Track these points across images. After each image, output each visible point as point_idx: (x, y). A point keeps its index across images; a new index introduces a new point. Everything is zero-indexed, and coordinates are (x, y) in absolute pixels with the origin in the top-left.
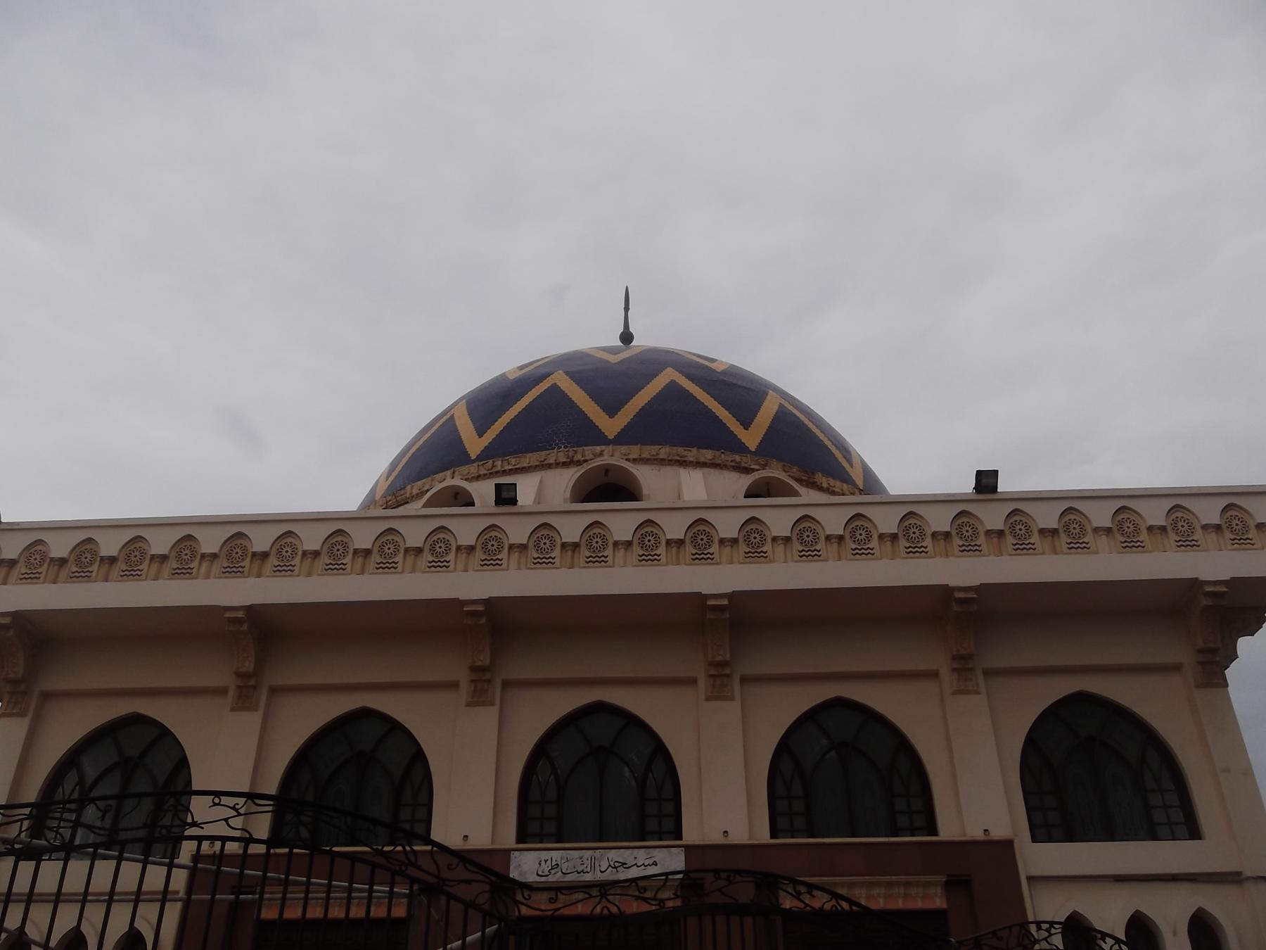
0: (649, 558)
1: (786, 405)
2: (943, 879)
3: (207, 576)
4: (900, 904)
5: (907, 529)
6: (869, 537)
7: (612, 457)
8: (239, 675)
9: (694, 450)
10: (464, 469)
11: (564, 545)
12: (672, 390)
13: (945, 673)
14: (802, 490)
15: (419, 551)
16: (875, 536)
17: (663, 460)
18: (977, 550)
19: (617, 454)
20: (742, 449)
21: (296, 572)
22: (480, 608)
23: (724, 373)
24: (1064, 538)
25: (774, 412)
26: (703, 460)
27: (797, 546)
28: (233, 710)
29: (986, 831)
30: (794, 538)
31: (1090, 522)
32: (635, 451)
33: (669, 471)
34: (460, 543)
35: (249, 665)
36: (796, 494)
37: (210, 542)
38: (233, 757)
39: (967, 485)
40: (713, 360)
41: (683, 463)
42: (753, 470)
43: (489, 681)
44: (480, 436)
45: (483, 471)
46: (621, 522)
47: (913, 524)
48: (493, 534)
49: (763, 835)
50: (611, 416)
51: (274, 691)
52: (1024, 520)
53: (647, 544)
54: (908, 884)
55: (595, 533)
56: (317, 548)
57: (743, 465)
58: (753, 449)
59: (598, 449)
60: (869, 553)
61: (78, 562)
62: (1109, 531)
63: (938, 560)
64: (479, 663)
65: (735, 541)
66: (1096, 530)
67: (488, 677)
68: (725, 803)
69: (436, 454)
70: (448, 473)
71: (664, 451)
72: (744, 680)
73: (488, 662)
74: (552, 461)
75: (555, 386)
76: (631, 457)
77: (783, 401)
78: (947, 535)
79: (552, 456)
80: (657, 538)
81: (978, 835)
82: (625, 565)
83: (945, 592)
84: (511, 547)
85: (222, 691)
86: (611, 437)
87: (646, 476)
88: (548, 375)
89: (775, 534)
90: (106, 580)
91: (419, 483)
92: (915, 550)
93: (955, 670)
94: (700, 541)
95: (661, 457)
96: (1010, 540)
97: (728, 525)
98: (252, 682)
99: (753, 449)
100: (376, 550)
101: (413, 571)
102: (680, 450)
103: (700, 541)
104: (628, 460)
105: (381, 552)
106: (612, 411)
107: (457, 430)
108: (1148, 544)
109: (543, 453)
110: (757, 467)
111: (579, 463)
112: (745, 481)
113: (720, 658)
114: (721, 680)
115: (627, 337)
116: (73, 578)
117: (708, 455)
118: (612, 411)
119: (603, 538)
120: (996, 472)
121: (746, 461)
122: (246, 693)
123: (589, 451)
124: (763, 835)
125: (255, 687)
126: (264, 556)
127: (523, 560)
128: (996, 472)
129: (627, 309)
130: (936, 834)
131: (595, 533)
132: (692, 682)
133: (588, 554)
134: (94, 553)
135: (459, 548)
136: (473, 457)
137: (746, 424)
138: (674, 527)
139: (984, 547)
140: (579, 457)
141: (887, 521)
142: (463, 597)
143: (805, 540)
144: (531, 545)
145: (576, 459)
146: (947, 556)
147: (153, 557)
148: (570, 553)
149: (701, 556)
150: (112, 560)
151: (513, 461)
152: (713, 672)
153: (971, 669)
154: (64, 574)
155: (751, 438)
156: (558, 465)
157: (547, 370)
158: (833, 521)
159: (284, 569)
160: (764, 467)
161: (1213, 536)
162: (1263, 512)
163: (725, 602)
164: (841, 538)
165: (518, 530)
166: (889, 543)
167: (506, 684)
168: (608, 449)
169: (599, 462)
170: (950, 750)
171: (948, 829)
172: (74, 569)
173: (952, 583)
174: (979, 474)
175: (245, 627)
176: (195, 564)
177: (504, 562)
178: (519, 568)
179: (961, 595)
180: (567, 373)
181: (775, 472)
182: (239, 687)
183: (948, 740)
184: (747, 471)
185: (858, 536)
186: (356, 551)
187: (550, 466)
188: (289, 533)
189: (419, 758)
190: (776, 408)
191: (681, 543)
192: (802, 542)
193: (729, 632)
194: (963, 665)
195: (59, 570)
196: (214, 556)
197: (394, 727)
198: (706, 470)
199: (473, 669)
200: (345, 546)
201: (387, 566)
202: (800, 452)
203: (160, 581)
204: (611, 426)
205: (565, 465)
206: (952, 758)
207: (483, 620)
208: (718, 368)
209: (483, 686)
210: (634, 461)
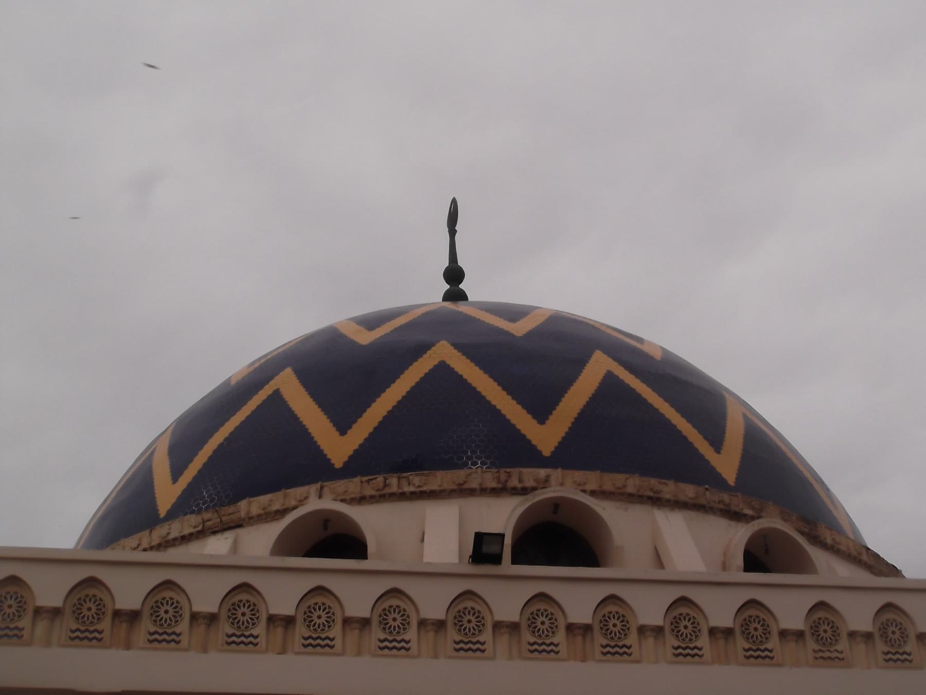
3: (48, 644)
7: (564, 486)
9: (671, 483)
14: (816, 554)
16: (775, 633)
17: (631, 495)
21: (182, 645)
25: (742, 431)
26: (682, 498)
27: (452, 634)
30: (596, 628)
31: (913, 623)
32: (593, 479)
41: (656, 501)
45: (369, 491)
52: (831, 618)
55: (753, 615)
56: (214, 609)
57: (733, 508)
60: (403, 648)
62: (868, 636)
66: (852, 635)
70: (313, 489)
71: (633, 483)
74: (474, 484)
75: (442, 370)
76: (590, 487)
78: (587, 628)
80: (177, 608)
86: (338, 463)
87: (371, 520)
88: (420, 350)
95: (630, 489)
97: (720, 609)
100: (146, 612)
102: (653, 482)
104: (584, 491)
106: (542, 412)
107: (295, 418)
108: (707, 652)
110: (749, 512)
111: (524, 491)
118: (541, 413)
126: (133, 616)
129: (452, 232)
131: (753, 615)
133: (605, 642)
139: (563, 648)
140: (514, 482)
146: (584, 660)
156: (484, 491)
161: (650, 641)
162: (925, 616)
174: (480, 538)
180: (456, 346)
187: (472, 492)
188: (168, 584)
192: (460, 628)
196: (56, 612)
198: (692, 514)
200: (254, 609)
205: (496, 492)
210: (593, 493)
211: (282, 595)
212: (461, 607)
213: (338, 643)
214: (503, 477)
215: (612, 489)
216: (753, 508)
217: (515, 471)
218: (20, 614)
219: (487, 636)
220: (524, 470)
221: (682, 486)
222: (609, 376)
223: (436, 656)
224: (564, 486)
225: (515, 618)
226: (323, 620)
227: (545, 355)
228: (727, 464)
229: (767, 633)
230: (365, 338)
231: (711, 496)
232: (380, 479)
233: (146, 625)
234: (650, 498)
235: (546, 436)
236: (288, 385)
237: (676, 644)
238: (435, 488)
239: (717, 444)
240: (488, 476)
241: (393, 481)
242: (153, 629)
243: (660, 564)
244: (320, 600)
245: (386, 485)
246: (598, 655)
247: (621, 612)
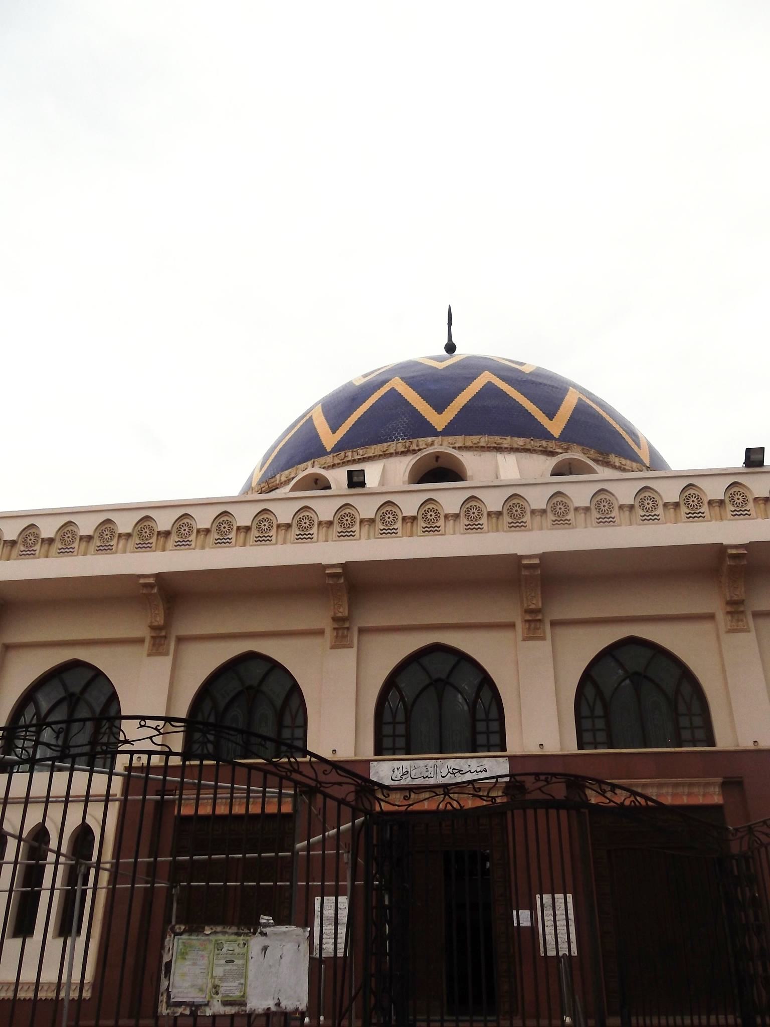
0: (473, 527)
1: (584, 399)
2: (720, 780)
3: (124, 552)
4: (685, 801)
6: (655, 506)
7: (442, 446)
8: (153, 628)
9: (509, 438)
10: (322, 460)
11: (404, 519)
12: (489, 390)
13: (720, 616)
15: (288, 526)
18: (747, 514)
19: (445, 443)
20: (548, 436)
22: (339, 571)
23: (531, 374)
26: (515, 446)
27: (595, 514)
28: (149, 655)
29: (755, 742)
32: (459, 440)
33: (488, 456)
34: (320, 519)
35: (160, 620)
36: (591, 471)
38: (152, 690)
39: (738, 461)
40: (522, 364)
41: (499, 449)
42: (557, 453)
43: (348, 628)
44: (334, 432)
45: (337, 461)
46: (449, 498)
47: (691, 497)
48: (347, 511)
49: (572, 747)
50: (440, 413)
51: (180, 640)
52: (564, 500)
53: (472, 515)
54: (691, 785)
55: (429, 510)
56: (208, 526)
57: (549, 449)
58: (557, 435)
59: (430, 440)
61: (25, 543)
64: (340, 615)
65: (544, 512)
67: (347, 625)
68: (540, 721)
69: (301, 448)
70: (310, 463)
71: (484, 440)
72: (554, 624)
73: (346, 614)
74: (392, 451)
75: (393, 391)
76: (457, 445)
77: (581, 396)
79: (393, 447)
81: (750, 746)
82: (454, 533)
83: (720, 550)
84: (362, 521)
85: (140, 641)
86: (440, 430)
87: (470, 461)
90: (47, 557)
91: (287, 472)
92: (695, 515)
93: (728, 613)
94: (515, 512)
95: (482, 444)
97: (537, 499)
98: (163, 633)
99: (557, 435)
101: (284, 542)
102: (497, 438)
103: (515, 512)
104: (454, 448)
105: (259, 528)
106: (440, 408)
109: (386, 445)
111: (414, 452)
112: (550, 463)
113: (533, 607)
114: (534, 624)
115: (450, 348)
116: (22, 555)
117: (519, 442)
118: (440, 408)
119: (436, 512)
120: (762, 450)
121: (551, 446)
122: (159, 641)
123: (422, 441)
124: (572, 747)
125: (165, 637)
126: (167, 534)
127: (372, 534)
128: (762, 450)
129: (450, 324)
130: (714, 745)
131: (429, 510)
132: (511, 626)
134: (37, 536)
135: (320, 523)
136: (329, 450)
137: (551, 416)
138: (493, 501)
139: (752, 512)
140: (414, 447)
141: (670, 492)
142: (325, 562)
143: (602, 508)
144: (378, 519)
145: (412, 448)
146: (722, 519)
147: (81, 538)
148: (409, 524)
149: (517, 524)
150: (51, 541)
151: (361, 452)
152: (528, 617)
153: (742, 612)
154: (15, 552)
155: (556, 427)
156: (397, 454)
157: (383, 377)
158: (625, 493)
159: (184, 543)
160: (566, 450)
163: (537, 561)
164: (632, 507)
165: (367, 508)
166: (672, 510)
167: (362, 631)
168: (437, 440)
169: (431, 450)
170: (725, 678)
171: (724, 741)
172: (22, 548)
173: (726, 542)
174: (748, 451)
175: (155, 590)
176: (114, 542)
177: (357, 533)
178: (369, 538)
179: (734, 551)
180: (402, 379)
181: (576, 454)
182: (152, 637)
183: (724, 671)
184: (552, 454)
185: (646, 505)
186: (238, 528)
187: (391, 455)
189: (295, 689)
191: (499, 514)
193: (538, 587)
194: (735, 608)
195: (11, 551)
196: (129, 535)
197: (275, 666)
198: (518, 454)
199: (335, 619)
200: (230, 524)
201: (264, 539)
202: (597, 437)
203: (89, 556)
204: (439, 421)
205: (403, 453)
206: (726, 684)
207: (342, 580)
208: (527, 369)
209: (343, 631)
210: (460, 448)
211: (410, 505)
212: (468, 506)
213: (315, 536)
214: (407, 445)
215: (471, 445)
216: (562, 448)
217: (415, 441)
219: (527, 517)
220: (420, 439)
221: (516, 439)
223: (631, 524)
225: (721, 497)
226: (696, 502)
232: (343, 453)
233: (174, 537)
234: (495, 448)
237: (688, 511)
238: (371, 455)
240: (400, 445)
241: (349, 454)
242: (467, 523)
244: (389, 508)
245: (345, 456)
246: (595, 524)
247: (697, 493)
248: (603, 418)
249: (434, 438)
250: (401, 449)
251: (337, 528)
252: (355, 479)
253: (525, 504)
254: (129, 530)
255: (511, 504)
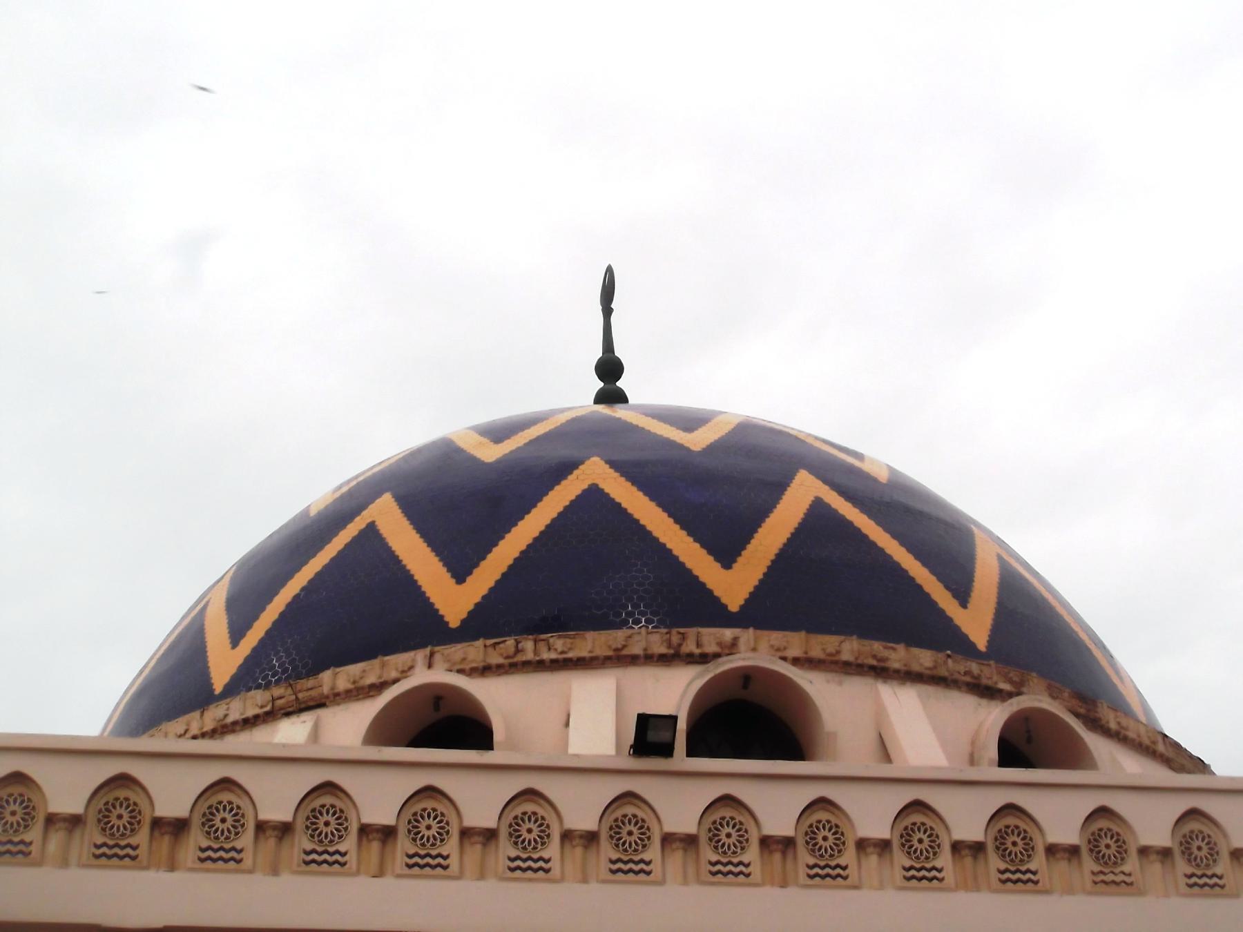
3: (64, 863)
5: (316, 813)
7: (757, 651)
9: (901, 648)
14: (1095, 743)
16: (1040, 849)
17: (847, 664)
19: (763, 646)
24: (805, 857)
26: (916, 667)
32: (796, 642)
37: (67, 791)
41: (881, 672)
44: (460, 578)
45: (495, 659)
52: (1115, 828)
56: (287, 816)
57: (984, 681)
58: (980, 640)
60: (541, 868)
62: (1165, 853)
63: (963, 898)
70: (420, 656)
71: (849, 648)
80: (238, 816)
87: (498, 697)
89: (367, 819)
95: (846, 656)
96: (805, 857)
97: (966, 817)
102: (877, 646)
104: (784, 659)
106: (727, 554)
107: (396, 560)
108: (949, 874)
118: (727, 554)
121: (990, 674)
126: (179, 827)
127: (691, 871)
129: (607, 312)
139: (755, 869)
140: (690, 647)
146: (784, 885)
151: (559, 644)
156: (649, 659)
161: (1156, 868)
162: (1242, 827)
174: (644, 721)
180: (613, 464)
187: (633, 660)
188: (225, 784)
190: (995, 564)
196: (75, 821)
205: (665, 660)
210: (796, 661)
211: (379, 798)
212: (619, 814)
213: (454, 862)
214: (675, 639)
215: (821, 655)
216: (1011, 682)
217: (691, 632)
218: (26, 824)
221: (916, 651)
222: (818, 504)
224: (757, 651)
227: (726, 481)
228: (976, 622)
229: (1029, 849)
230: (490, 453)
231: (956, 666)
232: (510, 642)
233: (196, 838)
235: (733, 584)
236: (387, 516)
238: (584, 654)
239: (962, 595)
243: (887, 757)
244: (429, 804)
245: (518, 651)
247: (834, 820)
248: (1026, 580)
249: (736, 631)
250: (658, 646)
251: (607, 851)
252: (652, 736)
253: (939, 830)
254: (77, 807)
255: (110, 797)
